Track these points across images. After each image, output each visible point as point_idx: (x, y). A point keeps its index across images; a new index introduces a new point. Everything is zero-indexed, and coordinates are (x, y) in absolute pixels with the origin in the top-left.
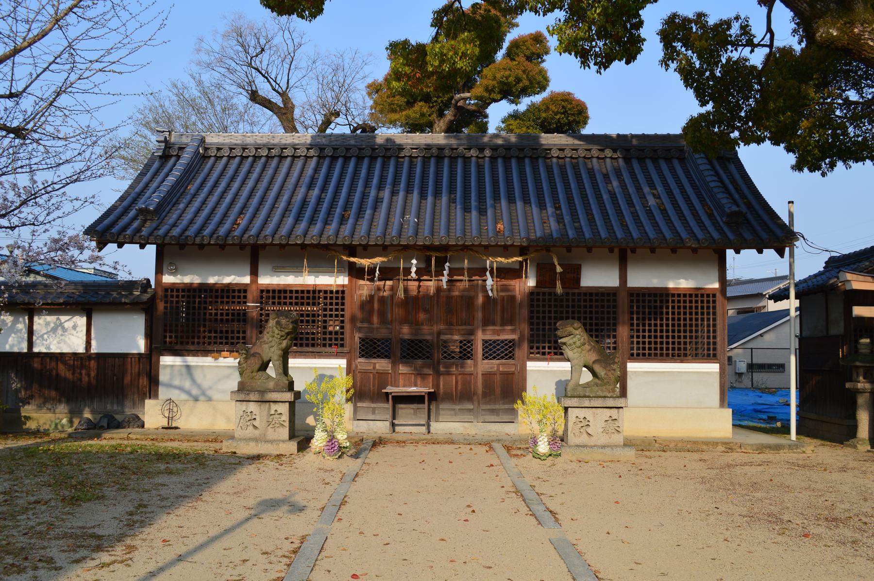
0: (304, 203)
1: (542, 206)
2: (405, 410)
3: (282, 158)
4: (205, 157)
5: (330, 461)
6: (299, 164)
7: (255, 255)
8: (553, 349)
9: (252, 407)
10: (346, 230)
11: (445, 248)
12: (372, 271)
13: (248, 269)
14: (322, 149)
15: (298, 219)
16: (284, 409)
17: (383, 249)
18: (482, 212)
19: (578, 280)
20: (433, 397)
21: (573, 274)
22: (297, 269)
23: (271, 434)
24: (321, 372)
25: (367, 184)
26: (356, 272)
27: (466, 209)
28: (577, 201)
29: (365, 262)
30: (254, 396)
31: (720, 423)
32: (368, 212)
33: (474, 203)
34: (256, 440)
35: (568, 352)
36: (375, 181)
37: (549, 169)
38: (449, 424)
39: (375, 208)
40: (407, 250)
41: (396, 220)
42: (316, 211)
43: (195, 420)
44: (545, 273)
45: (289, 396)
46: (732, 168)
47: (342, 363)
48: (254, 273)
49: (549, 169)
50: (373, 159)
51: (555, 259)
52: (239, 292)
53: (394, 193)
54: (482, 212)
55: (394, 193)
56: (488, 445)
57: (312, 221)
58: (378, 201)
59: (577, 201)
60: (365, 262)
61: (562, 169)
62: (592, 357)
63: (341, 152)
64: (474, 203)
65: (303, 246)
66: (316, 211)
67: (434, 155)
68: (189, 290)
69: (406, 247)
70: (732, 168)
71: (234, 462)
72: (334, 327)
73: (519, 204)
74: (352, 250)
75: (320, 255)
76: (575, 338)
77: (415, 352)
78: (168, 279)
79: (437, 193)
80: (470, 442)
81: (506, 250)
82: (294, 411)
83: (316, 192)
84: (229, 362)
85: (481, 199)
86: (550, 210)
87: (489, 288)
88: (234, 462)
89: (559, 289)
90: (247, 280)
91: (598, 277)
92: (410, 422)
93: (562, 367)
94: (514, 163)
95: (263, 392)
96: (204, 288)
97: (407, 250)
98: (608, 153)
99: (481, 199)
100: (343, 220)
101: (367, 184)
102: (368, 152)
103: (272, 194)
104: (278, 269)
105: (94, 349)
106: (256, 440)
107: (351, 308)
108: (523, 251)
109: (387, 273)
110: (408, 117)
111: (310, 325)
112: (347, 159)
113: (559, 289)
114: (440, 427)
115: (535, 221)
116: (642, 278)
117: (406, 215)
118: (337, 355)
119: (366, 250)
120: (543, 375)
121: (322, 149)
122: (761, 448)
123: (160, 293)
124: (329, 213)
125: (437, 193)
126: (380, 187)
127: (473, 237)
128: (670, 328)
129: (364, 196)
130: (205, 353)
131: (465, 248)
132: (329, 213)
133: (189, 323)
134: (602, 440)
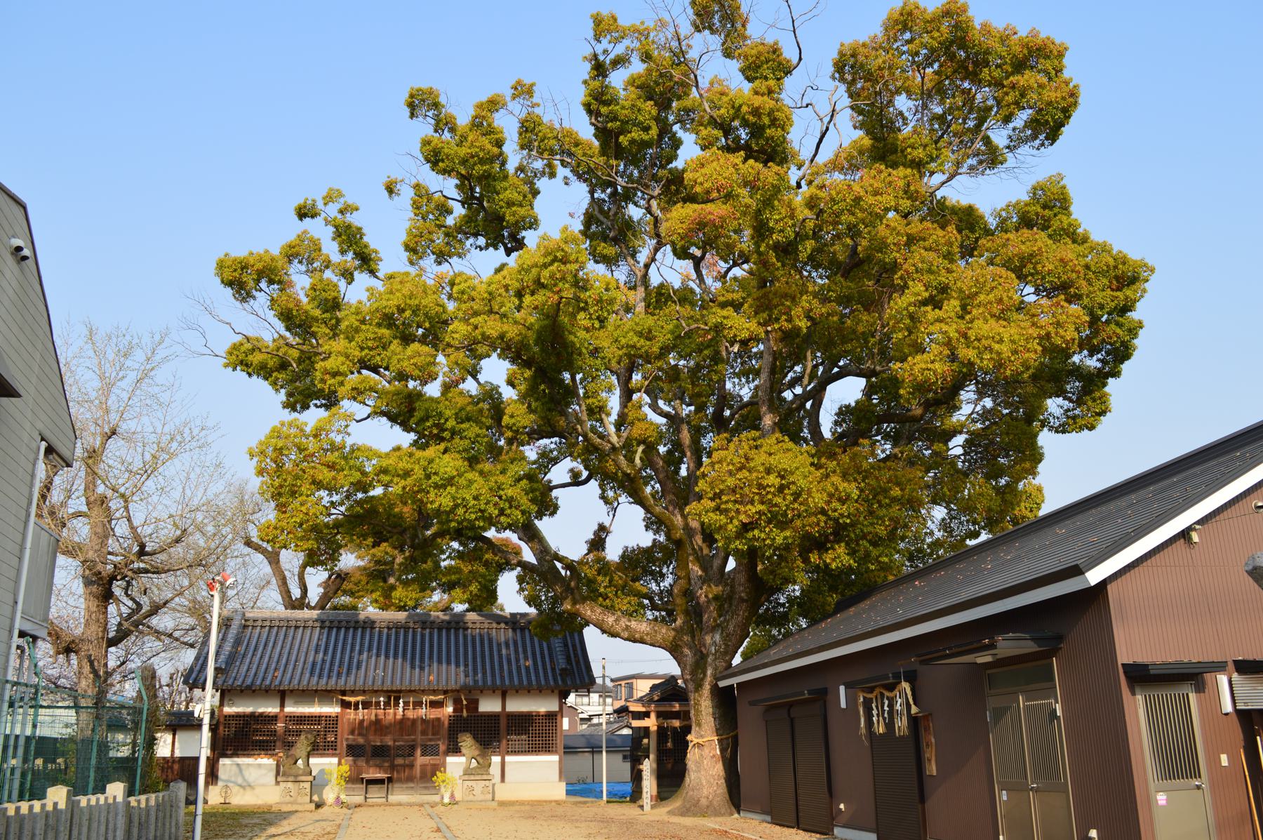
0: (314, 664)
1: (457, 665)
2: (372, 788)
3: (297, 627)
4: (245, 627)
5: (337, 809)
6: (308, 632)
7: (283, 696)
8: (455, 750)
9: (290, 785)
10: (342, 682)
11: (400, 691)
12: (356, 705)
13: (278, 703)
14: (323, 622)
15: (312, 674)
16: (307, 785)
17: (364, 692)
18: (422, 668)
19: (477, 708)
20: (390, 780)
21: (474, 704)
22: (311, 703)
23: (300, 800)
24: (325, 764)
25: (352, 650)
26: (346, 705)
27: (413, 667)
28: (479, 660)
29: (352, 699)
30: (291, 779)
31: (558, 791)
32: (354, 671)
33: (417, 663)
34: (292, 803)
35: (464, 750)
36: (357, 648)
37: (465, 637)
38: (400, 796)
39: (358, 668)
40: (376, 692)
41: (371, 673)
42: (322, 669)
43: (241, 799)
44: (457, 702)
45: (310, 778)
46: (576, 635)
47: (335, 760)
48: (282, 706)
49: (465, 637)
50: (355, 629)
51: (466, 697)
52: (273, 718)
53: (369, 657)
54: (422, 668)
55: (369, 657)
56: (421, 805)
57: (320, 676)
58: (359, 663)
59: (479, 660)
60: (352, 699)
61: (473, 638)
62: (477, 753)
63: (336, 624)
64: (417, 663)
65: (316, 691)
66: (322, 669)
67: (396, 627)
68: (238, 716)
69: (376, 691)
70: (576, 635)
71: (283, 816)
72: (331, 738)
73: (444, 666)
74: (344, 693)
75: (325, 695)
76: (467, 742)
77: (380, 753)
78: (228, 710)
79: (396, 657)
80: (411, 805)
81: (434, 692)
82: (1162, 544)
83: (321, 655)
84: (267, 762)
85: (422, 660)
86: (462, 668)
87: (617, 392)
88: (283, 816)
89: (465, 714)
90: (277, 710)
91: (489, 705)
92: (376, 794)
93: (463, 759)
94: (444, 632)
95: (296, 776)
96: (252, 715)
97: (376, 692)
98: (503, 625)
99: (422, 660)
100: (339, 675)
101: (352, 650)
102: (352, 624)
103: (286, 651)
104: (296, 703)
105: (178, 754)
106: (292, 803)
107: (343, 729)
108: (445, 692)
109: (366, 705)
110: (374, 555)
111: (322, 737)
112: (339, 629)
113: (465, 714)
114: (393, 798)
115: (454, 676)
116: (517, 705)
117: (378, 670)
118: (333, 755)
119: (353, 693)
120: (455, 764)
121: (323, 622)
122: (576, 803)
123: (222, 720)
124: (331, 670)
125: (396, 657)
126: (361, 653)
127: (415, 685)
128: (533, 734)
129: (351, 658)
130: (248, 756)
131: (410, 691)
132: (331, 670)
133: (237, 737)
134: (481, 797)
